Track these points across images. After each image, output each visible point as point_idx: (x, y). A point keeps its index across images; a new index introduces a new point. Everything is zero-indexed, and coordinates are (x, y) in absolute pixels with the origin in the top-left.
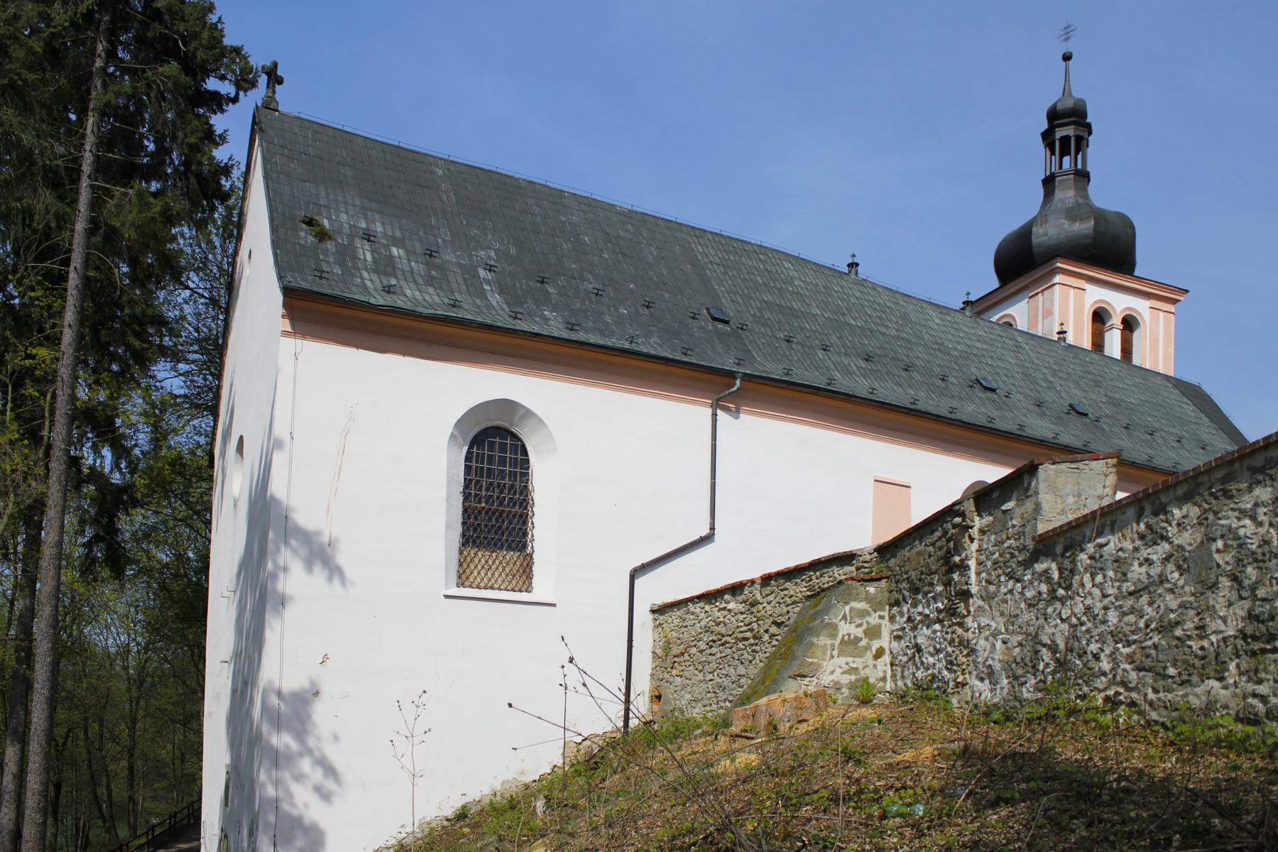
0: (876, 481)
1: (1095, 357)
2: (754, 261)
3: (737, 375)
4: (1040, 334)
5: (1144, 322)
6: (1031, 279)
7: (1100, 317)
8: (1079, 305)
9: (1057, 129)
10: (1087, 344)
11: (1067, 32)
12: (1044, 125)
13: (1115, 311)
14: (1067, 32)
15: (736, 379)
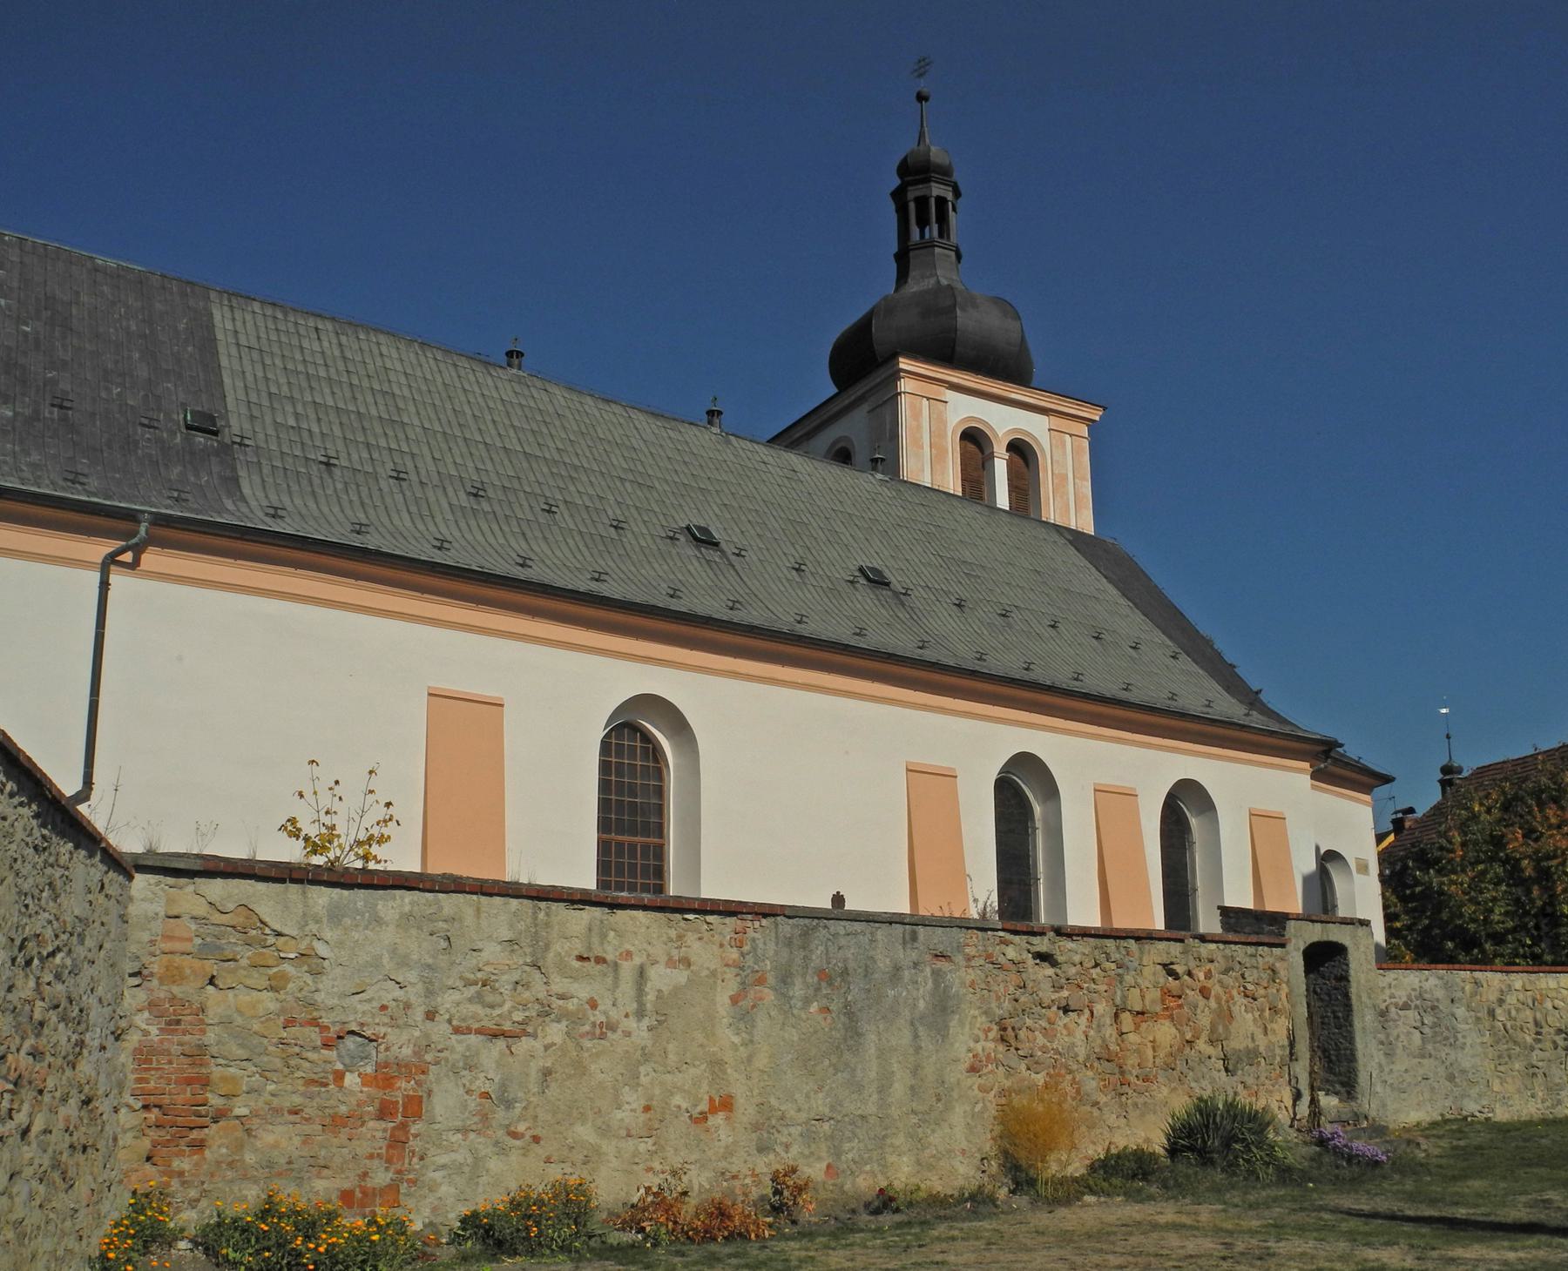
0: (430, 694)
1: (970, 511)
2: (682, 476)
3: (141, 517)
4: (952, 492)
5: (1042, 450)
6: (868, 388)
7: (974, 439)
8: (938, 422)
9: (910, 188)
10: (952, 482)
11: (922, 68)
12: (896, 182)
13: (996, 435)
14: (922, 68)
15: (139, 522)
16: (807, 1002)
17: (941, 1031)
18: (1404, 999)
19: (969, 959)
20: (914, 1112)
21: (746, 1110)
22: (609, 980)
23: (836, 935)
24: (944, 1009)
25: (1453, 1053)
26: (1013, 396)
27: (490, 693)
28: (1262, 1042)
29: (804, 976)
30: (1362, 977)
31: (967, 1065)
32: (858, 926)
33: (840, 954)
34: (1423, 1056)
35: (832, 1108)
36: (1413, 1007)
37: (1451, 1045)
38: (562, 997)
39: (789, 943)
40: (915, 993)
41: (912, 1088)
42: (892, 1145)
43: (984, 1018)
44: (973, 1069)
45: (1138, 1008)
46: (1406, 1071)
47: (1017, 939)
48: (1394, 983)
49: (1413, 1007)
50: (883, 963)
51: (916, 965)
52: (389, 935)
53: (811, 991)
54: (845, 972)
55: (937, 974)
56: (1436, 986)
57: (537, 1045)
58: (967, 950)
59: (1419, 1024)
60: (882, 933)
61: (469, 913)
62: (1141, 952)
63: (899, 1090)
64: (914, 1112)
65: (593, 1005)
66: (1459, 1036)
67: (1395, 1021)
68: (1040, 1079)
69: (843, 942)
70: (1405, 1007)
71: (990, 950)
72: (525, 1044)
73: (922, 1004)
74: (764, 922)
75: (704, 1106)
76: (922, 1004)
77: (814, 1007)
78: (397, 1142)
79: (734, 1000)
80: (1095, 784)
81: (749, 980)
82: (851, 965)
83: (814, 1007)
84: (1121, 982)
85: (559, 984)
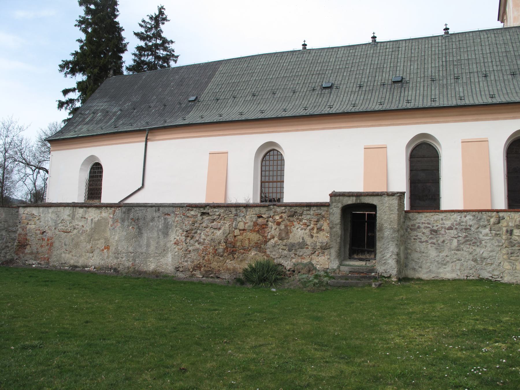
16: (128, 226)
17: (166, 234)
18: (449, 225)
19: (177, 215)
20: (156, 253)
21: (113, 249)
22: (86, 222)
23: (136, 210)
24: (167, 228)
25: (478, 249)
27: (224, 150)
28: (309, 241)
29: (128, 220)
31: (174, 242)
32: (142, 208)
33: (137, 215)
34: (458, 250)
35: (133, 250)
36: (454, 228)
37: (478, 246)
38: (77, 225)
39: (124, 213)
40: (158, 224)
41: (156, 247)
42: (149, 260)
43: (180, 230)
44: (175, 243)
45: (241, 228)
46: (447, 256)
47: (195, 209)
48: (444, 218)
49: (454, 228)
50: (149, 217)
51: (159, 217)
52: (50, 215)
53: (129, 224)
54: (138, 219)
55: (165, 219)
56: (470, 219)
57: (72, 234)
58: (176, 212)
59: (456, 236)
60: (149, 209)
61: (62, 210)
62: (247, 211)
63: (152, 247)
64: (156, 253)
65: (83, 226)
66: (483, 242)
67: (443, 234)
68: (201, 247)
69: (138, 212)
70: (450, 228)
71: (184, 212)
72: (70, 234)
73: (160, 227)
74: (119, 208)
75: (103, 248)
76: (160, 227)
77: (131, 227)
78: (50, 249)
79: (111, 226)
80: (462, 140)
81: (115, 221)
82: (140, 217)
83: (131, 227)
84: (236, 220)
85: (77, 223)
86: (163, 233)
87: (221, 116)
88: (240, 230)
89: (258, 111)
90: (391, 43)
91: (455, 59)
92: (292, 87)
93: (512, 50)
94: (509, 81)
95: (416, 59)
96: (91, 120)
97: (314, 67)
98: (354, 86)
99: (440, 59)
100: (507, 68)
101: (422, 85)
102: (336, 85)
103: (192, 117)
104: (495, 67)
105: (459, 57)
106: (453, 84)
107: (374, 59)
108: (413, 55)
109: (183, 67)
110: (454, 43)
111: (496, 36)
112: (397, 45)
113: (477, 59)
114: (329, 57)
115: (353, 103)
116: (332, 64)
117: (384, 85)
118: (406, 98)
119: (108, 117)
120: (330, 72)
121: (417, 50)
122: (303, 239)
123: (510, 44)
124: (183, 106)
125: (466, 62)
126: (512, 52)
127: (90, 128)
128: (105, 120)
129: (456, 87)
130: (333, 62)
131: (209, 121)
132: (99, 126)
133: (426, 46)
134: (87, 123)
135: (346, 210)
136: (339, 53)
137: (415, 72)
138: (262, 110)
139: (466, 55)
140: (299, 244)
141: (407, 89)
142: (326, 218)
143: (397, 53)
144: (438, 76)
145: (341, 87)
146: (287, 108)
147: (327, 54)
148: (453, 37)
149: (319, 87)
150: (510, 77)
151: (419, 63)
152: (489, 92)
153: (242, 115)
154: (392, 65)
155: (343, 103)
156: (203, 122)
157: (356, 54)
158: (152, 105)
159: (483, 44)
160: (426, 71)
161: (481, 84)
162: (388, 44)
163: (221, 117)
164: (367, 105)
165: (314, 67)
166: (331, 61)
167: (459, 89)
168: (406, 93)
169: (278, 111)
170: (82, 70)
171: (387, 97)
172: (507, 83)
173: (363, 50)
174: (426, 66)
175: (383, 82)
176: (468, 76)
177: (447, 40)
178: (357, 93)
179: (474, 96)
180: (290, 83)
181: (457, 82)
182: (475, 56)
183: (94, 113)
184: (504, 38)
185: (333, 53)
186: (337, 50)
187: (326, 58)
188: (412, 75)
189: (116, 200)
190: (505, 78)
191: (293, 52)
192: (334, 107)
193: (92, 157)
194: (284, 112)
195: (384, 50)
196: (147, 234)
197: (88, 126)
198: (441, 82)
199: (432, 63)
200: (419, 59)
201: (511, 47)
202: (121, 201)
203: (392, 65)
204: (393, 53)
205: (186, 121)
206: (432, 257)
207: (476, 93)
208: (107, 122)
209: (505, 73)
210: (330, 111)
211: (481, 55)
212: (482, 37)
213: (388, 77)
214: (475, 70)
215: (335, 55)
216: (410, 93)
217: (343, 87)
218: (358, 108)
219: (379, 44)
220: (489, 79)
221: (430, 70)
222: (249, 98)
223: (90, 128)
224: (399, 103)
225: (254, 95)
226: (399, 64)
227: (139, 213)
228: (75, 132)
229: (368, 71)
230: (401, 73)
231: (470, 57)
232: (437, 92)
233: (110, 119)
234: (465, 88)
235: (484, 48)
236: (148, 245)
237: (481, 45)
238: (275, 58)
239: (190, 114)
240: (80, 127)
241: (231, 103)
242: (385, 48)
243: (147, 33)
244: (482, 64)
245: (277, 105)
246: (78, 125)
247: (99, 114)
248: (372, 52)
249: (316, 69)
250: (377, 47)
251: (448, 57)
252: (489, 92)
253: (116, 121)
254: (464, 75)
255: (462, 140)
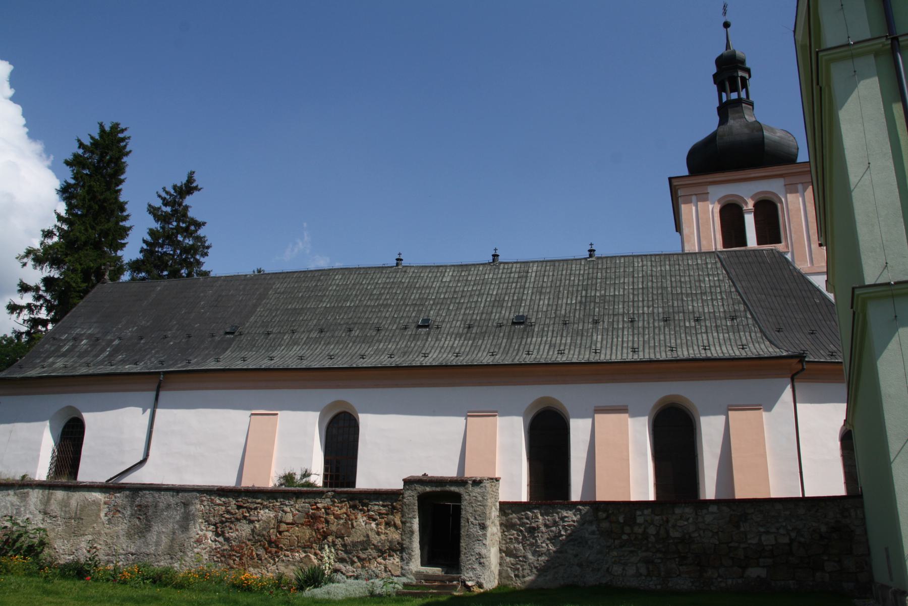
23: (145, 494)
24: (187, 519)
26: (753, 175)
28: (375, 539)
30: (470, 510)
45: (288, 521)
66: (589, 542)
86: (181, 526)
87: (272, 360)
88: (287, 524)
89: (325, 356)
90: (518, 265)
91: (598, 294)
92: (376, 321)
93: (669, 286)
94: (660, 330)
95: (548, 290)
96: (69, 351)
97: (410, 294)
98: (462, 326)
99: (579, 293)
100: (661, 310)
101: (551, 328)
102: (437, 324)
103: (230, 360)
104: (646, 309)
105: (603, 292)
106: (591, 330)
107: (492, 287)
108: (545, 285)
109: (220, 277)
110: (599, 271)
111: (654, 264)
112: (526, 269)
113: (626, 297)
114: (432, 280)
115: (457, 351)
116: (436, 291)
117: (501, 326)
118: (527, 349)
119: (99, 348)
120: (431, 302)
121: (551, 277)
122: (368, 536)
123: (668, 278)
124: (217, 338)
125: (611, 299)
126: (669, 289)
127: (69, 364)
128: (94, 353)
129: (594, 334)
130: (437, 288)
131: (254, 367)
132: (83, 361)
133: (564, 272)
134: (64, 355)
135: (423, 499)
136: (446, 275)
137: (545, 309)
138: (332, 354)
139: (612, 290)
140: (362, 543)
141: (530, 334)
142: (397, 510)
143: (524, 280)
144: (572, 317)
145: (444, 325)
146: (367, 353)
147: (430, 276)
148: (600, 262)
149: (414, 325)
150: (662, 324)
151: (551, 297)
152: (633, 344)
153: (302, 359)
154: (515, 298)
155: (443, 351)
156: (245, 367)
157: (469, 278)
158: (169, 334)
159: (636, 275)
160: (559, 309)
161: (626, 333)
162: (515, 265)
163: (273, 362)
164: (474, 356)
165: (410, 294)
166: (434, 286)
167: (597, 338)
168: (529, 340)
169: (354, 358)
170: (55, 262)
171: (503, 345)
172: (657, 331)
173: (479, 273)
174: (560, 302)
175: (500, 322)
176: (611, 320)
177: (591, 266)
178: (464, 336)
179: (614, 348)
180: (374, 316)
181: (596, 327)
182: (624, 292)
183: (75, 339)
184: (663, 269)
185: (439, 274)
186: (444, 271)
187: (428, 281)
188: (540, 314)
189: (102, 478)
190: (656, 324)
191: (382, 269)
192: (430, 356)
193: (71, 408)
194: (361, 359)
195: (508, 275)
196: (158, 527)
197: (66, 359)
198: (576, 326)
199: (568, 297)
200: (552, 292)
201: (669, 282)
202: (111, 479)
203: (515, 298)
204: (520, 280)
205: (221, 363)
206: (531, 561)
207: (617, 345)
208: (97, 356)
209: (656, 318)
210: (424, 362)
211: (631, 291)
212: (636, 264)
213: (508, 315)
214: (621, 311)
215: (440, 278)
216: (534, 339)
217: (446, 327)
218: (462, 358)
219: (502, 266)
220: (636, 324)
221: (564, 307)
222: (314, 335)
223: (69, 364)
224: (517, 354)
225: (321, 331)
226: (524, 297)
227: (148, 498)
228: (43, 368)
229: (482, 305)
230: (526, 310)
231: (617, 293)
232: (569, 341)
233: (103, 350)
234: (605, 337)
235: (635, 280)
236: (157, 544)
237: (633, 277)
238: (356, 275)
239: (227, 352)
240: (51, 360)
241: (287, 341)
242: (509, 271)
243: (307, 556)
244: (631, 304)
245: (353, 348)
246: (48, 357)
247: (84, 342)
248: (491, 276)
249: (412, 297)
250: (499, 269)
251: (589, 291)
252: (633, 344)
253: (111, 355)
254: (606, 318)
255: (595, 407)
